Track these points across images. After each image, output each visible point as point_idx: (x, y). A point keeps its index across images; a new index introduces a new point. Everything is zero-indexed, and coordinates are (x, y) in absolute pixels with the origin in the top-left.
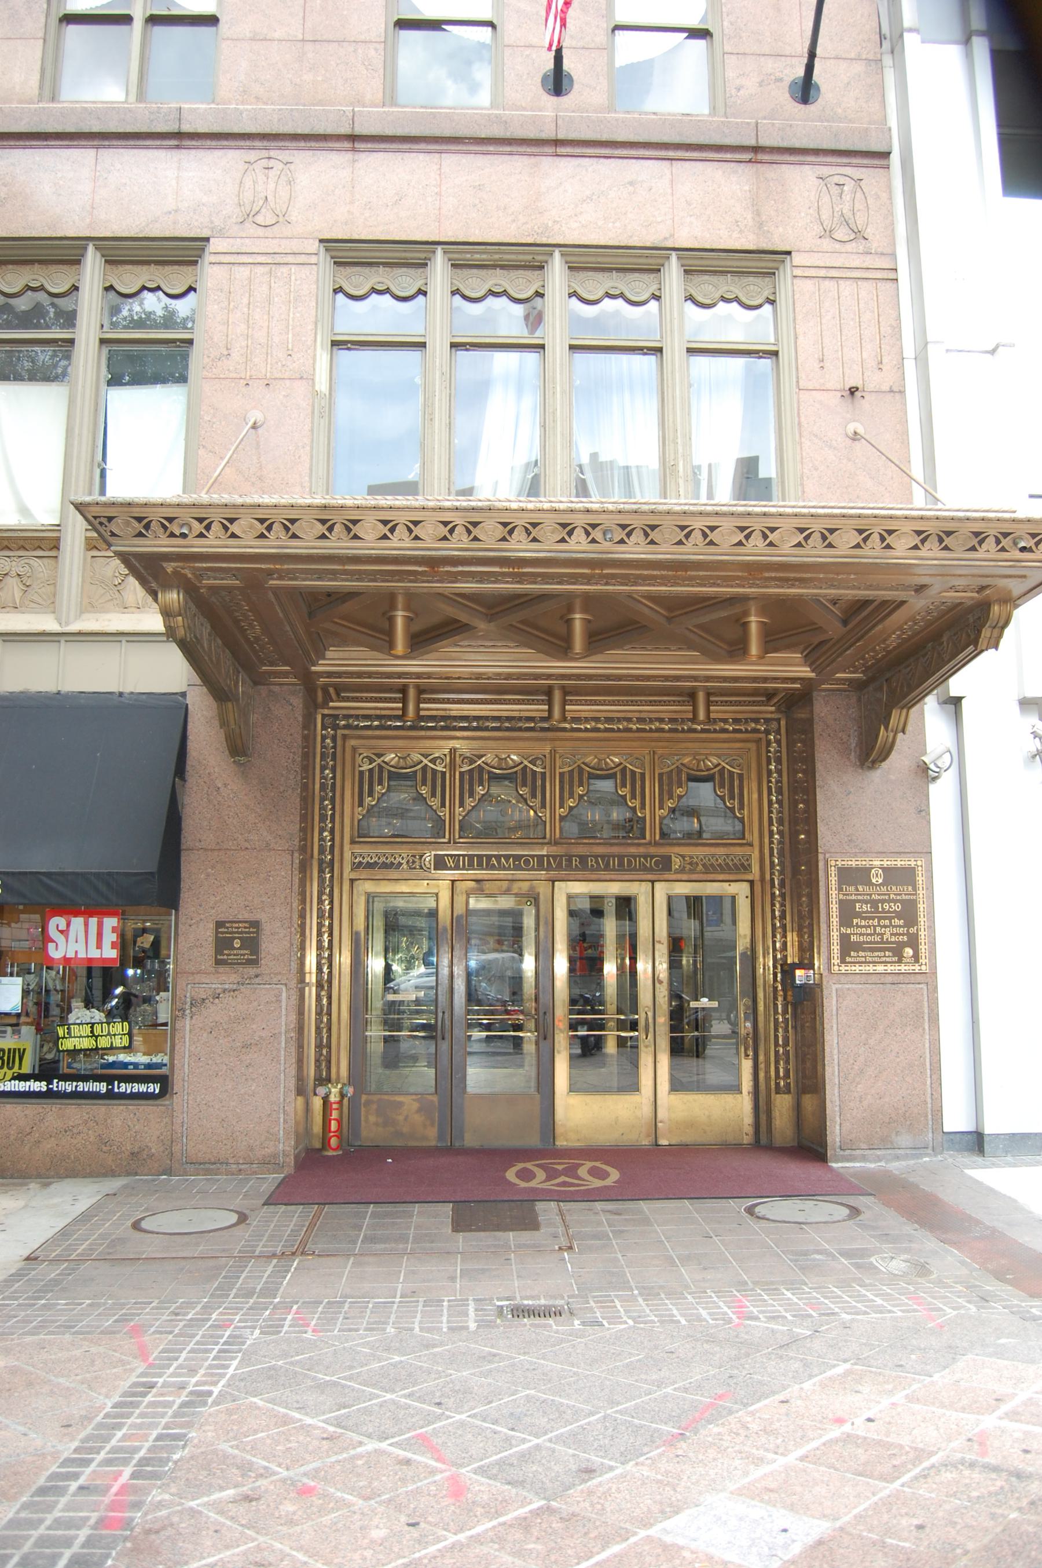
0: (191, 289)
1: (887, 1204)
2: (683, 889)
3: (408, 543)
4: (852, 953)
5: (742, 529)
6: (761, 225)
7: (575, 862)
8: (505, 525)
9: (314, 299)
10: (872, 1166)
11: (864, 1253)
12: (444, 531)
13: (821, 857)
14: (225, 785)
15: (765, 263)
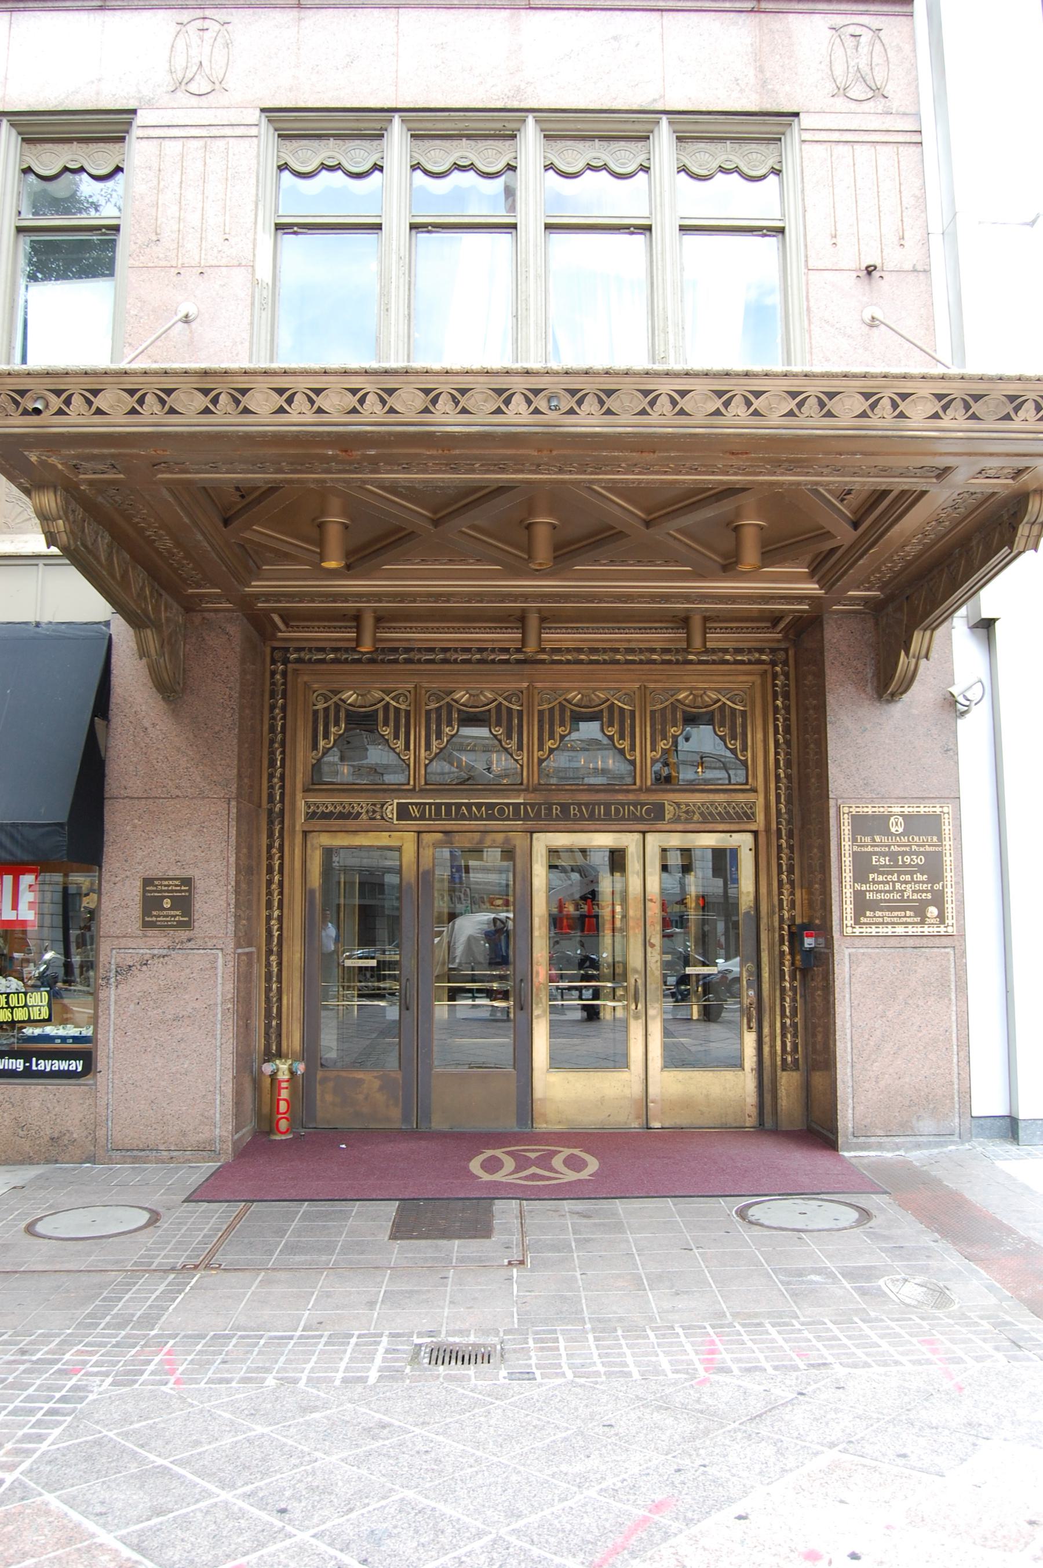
0: (118, 169)
1: (904, 1205)
2: (675, 840)
3: (310, 417)
4: (868, 914)
5: (720, 394)
6: (764, 83)
7: (556, 810)
8: (427, 391)
9: (254, 176)
10: (889, 1155)
11: (869, 1273)
12: (352, 401)
13: (832, 803)
14: (154, 725)
15: (770, 127)
